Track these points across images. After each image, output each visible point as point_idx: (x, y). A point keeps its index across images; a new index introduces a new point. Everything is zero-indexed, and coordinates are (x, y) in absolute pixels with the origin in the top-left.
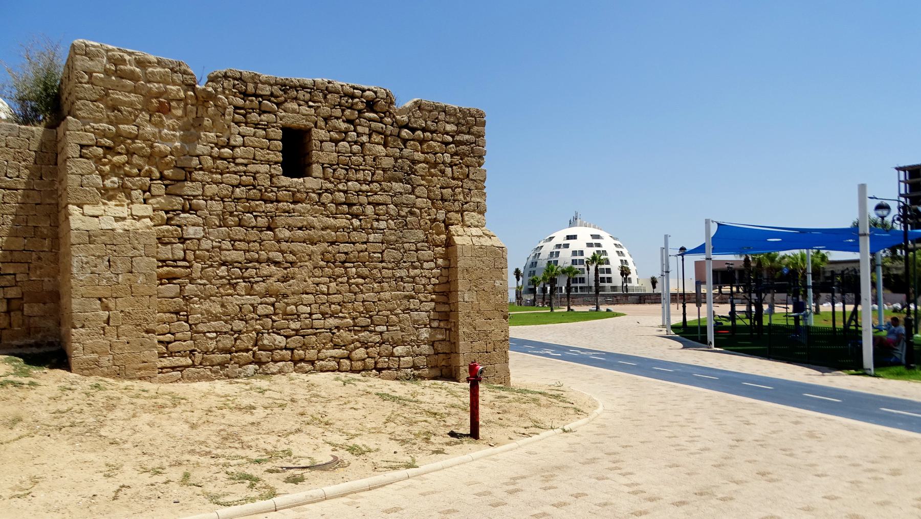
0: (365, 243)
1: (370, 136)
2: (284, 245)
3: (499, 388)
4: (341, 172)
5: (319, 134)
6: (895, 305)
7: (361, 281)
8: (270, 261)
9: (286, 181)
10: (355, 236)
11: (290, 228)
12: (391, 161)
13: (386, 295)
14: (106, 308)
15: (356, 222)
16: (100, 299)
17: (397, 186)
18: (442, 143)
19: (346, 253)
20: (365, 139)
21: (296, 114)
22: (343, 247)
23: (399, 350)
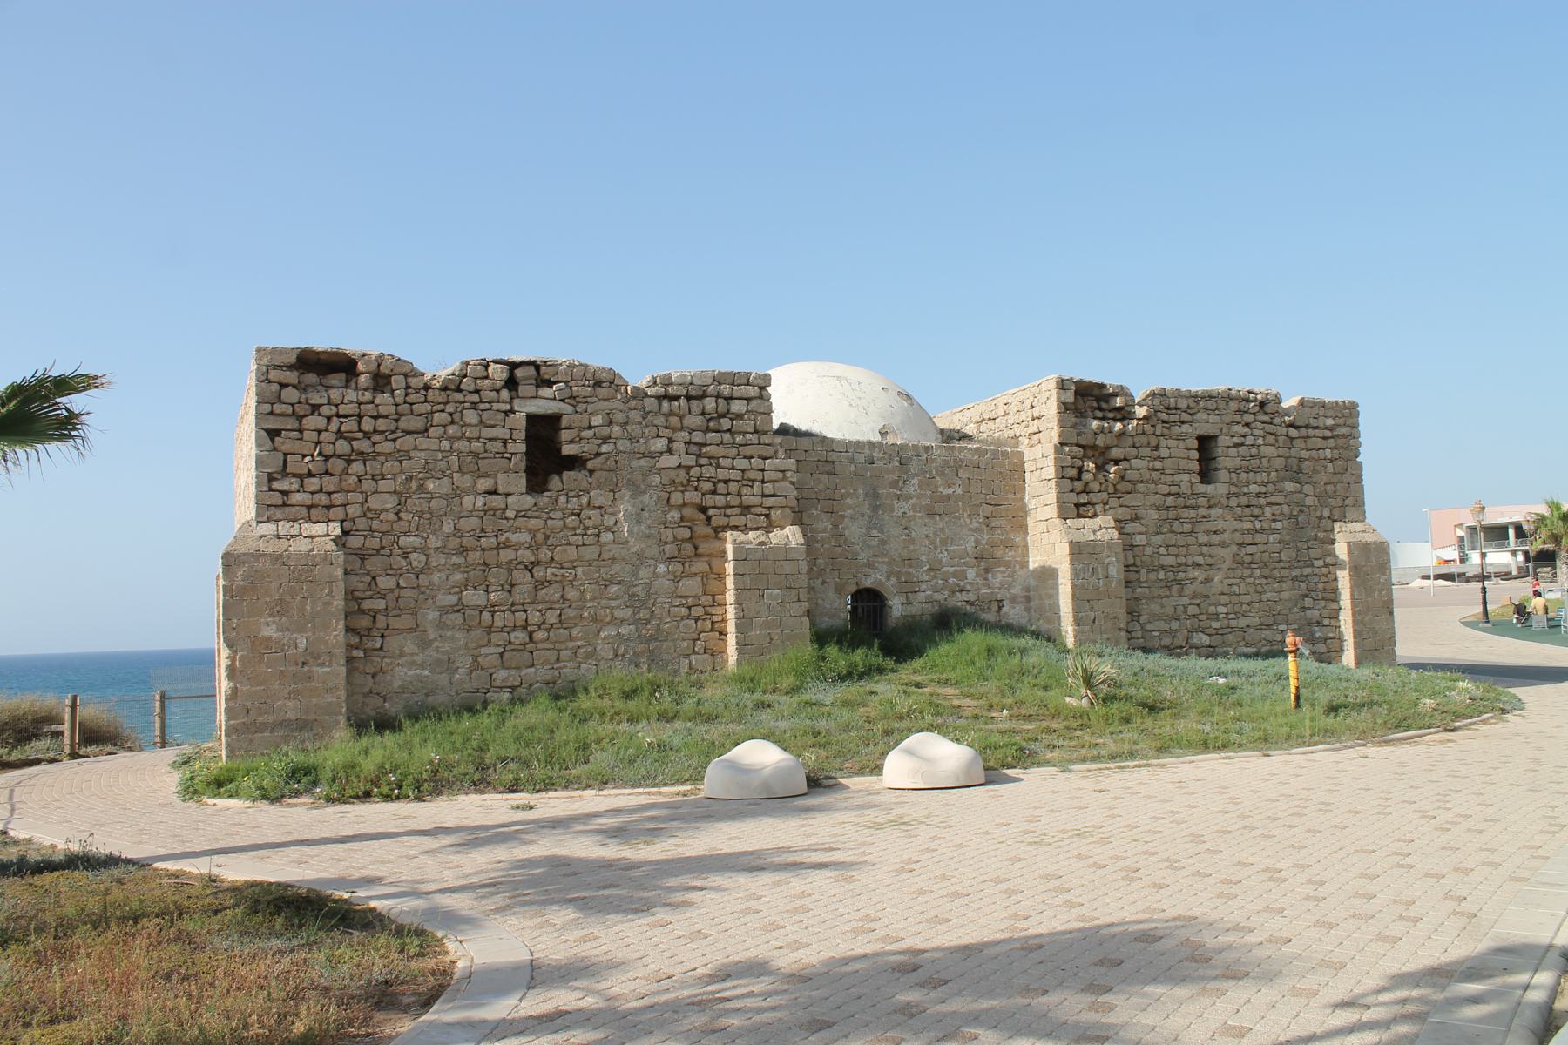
9: (1202, 488)
10: (1259, 538)
11: (1208, 533)
13: (1285, 595)
20: (1260, 441)
21: (1206, 424)
22: (1250, 549)
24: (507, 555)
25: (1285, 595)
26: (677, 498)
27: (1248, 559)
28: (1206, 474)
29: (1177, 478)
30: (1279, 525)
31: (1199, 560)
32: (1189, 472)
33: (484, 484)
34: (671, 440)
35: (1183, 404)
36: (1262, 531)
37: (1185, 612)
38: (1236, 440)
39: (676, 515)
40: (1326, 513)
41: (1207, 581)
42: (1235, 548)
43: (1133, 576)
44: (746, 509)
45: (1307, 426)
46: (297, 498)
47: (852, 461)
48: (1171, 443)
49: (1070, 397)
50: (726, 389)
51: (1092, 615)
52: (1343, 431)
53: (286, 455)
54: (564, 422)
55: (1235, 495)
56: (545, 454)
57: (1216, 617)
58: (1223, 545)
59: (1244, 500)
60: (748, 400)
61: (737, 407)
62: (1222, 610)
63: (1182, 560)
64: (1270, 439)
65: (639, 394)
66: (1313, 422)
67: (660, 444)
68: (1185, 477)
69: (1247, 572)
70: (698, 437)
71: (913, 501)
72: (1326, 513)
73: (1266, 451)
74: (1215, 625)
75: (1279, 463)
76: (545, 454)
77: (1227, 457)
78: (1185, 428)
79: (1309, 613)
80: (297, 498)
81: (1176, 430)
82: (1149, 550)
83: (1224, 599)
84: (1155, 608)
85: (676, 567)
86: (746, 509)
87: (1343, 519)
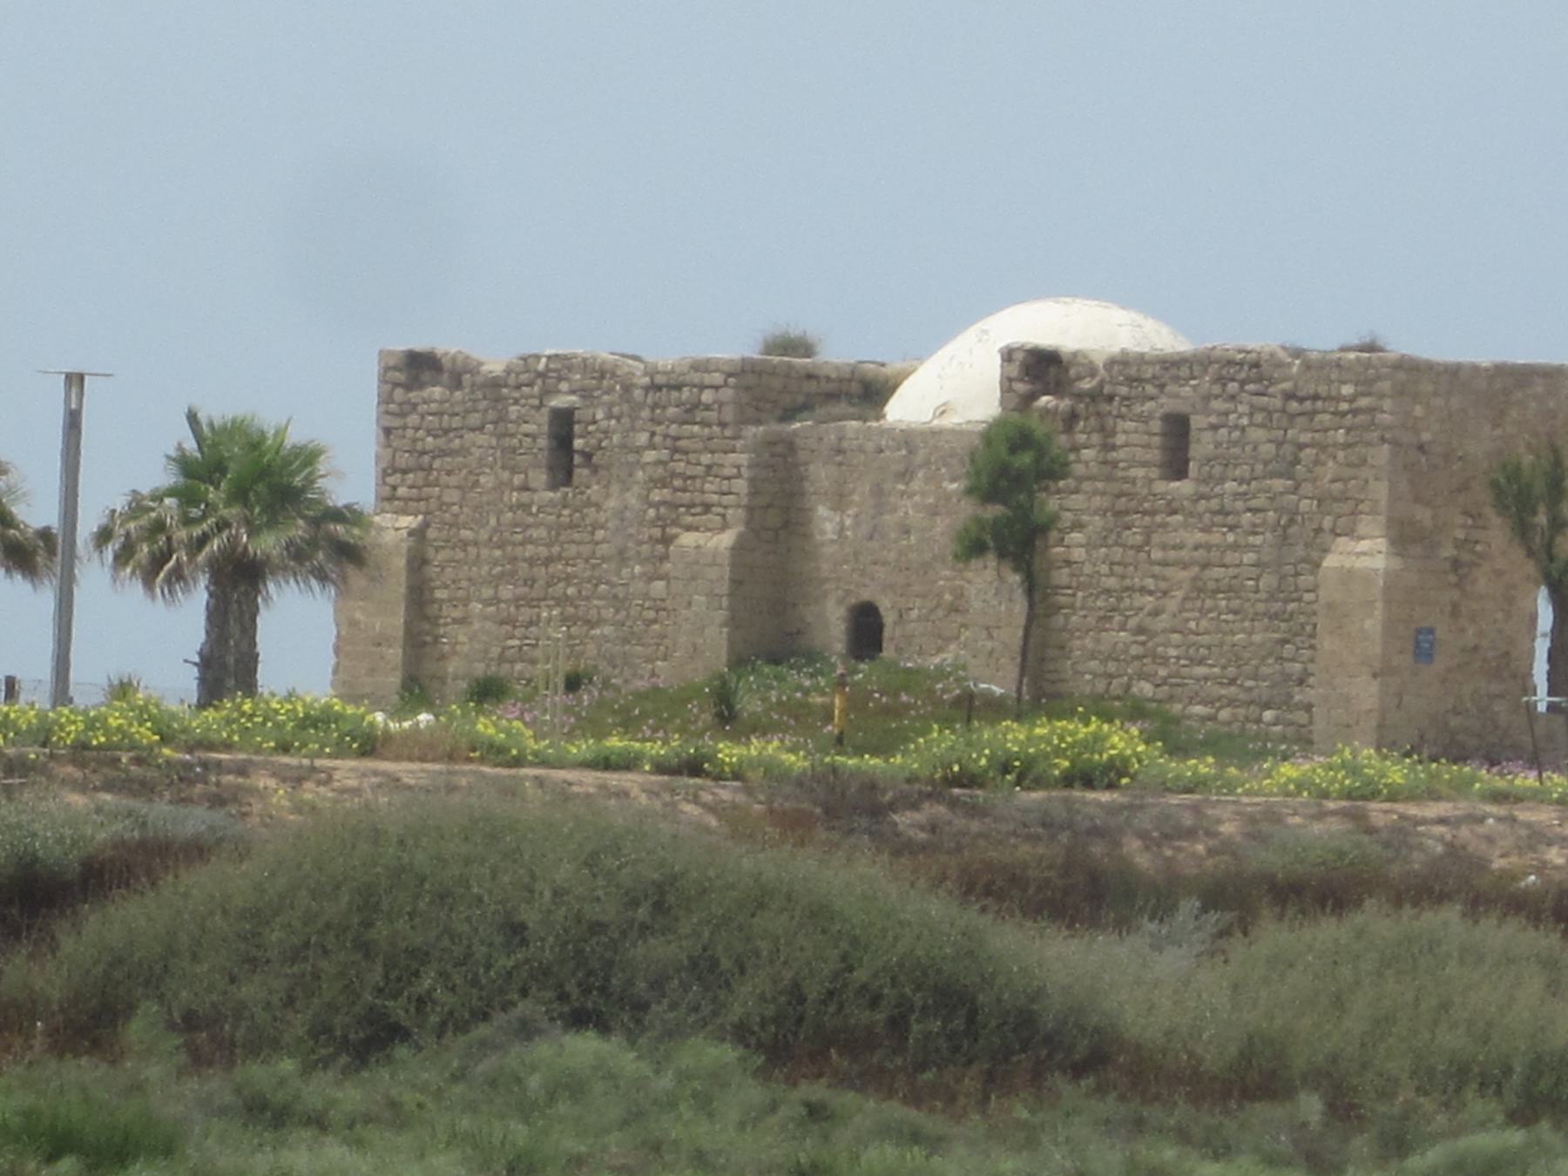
0: (1238, 566)
1: (1251, 415)
2: (1157, 569)
3: (211, 747)
4: (1217, 470)
5: (1197, 421)
6: (206, 967)
7: (1230, 617)
8: (1143, 590)
9: (1160, 487)
10: (1230, 557)
11: (1164, 547)
12: (1271, 448)
13: (1257, 638)
14: (990, 637)
15: (1231, 538)
16: (987, 628)
17: (1279, 484)
18: (1334, 414)
19: (1217, 580)
20: (1245, 421)
21: (1181, 397)
22: (1217, 572)
23: (1268, 715)
24: (530, 550)
25: (1257, 638)
26: (656, 496)
27: (1211, 585)
28: (1177, 468)
29: (1133, 472)
30: (1258, 540)
31: (1150, 583)
32: (1144, 464)
33: (518, 480)
34: (653, 434)
35: (1149, 372)
36: (1235, 547)
37: (1126, 651)
38: (1213, 419)
39: (652, 512)
40: (1327, 522)
41: (1156, 613)
42: (1197, 569)
43: (660, 548)
44: (707, 508)
45: (1316, 397)
46: (402, 491)
47: (861, 449)
48: (1130, 425)
49: (1014, 370)
50: (696, 377)
51: (989, 644)
52: (1363, 402)
53: (395, 451)
54: (577, 415)
55: (1202, 497)
56: (564, 450)
57: (1165, 661)
58: (1185, 566)
59: (1214, 504)
60: (716, 388)
61: (707, 396)
62: (1173, 652)
63: (1128, 582)
64: (1259, 418)
65: (495, 384)
66: (1322, 390)
67: (643, 438)
68: (1139, 472)
69: (1209, 603)
70: (674, 429)
71: (917, 498)
72: (1327, 522)
73: (1256, 434)
74: (1162, 672)
75: (1268, 450)
76: (564, 450)
77: (1202, 446)
78: (1149, 405)
79: (1288, 665)
80: (402, 491)
81: (1138, 409)
82: (1088, 569)
83: (1176, 637)
84: (1089, 642)
85: (649, 568)
86: (707, 508)
87: (1350, 533)
